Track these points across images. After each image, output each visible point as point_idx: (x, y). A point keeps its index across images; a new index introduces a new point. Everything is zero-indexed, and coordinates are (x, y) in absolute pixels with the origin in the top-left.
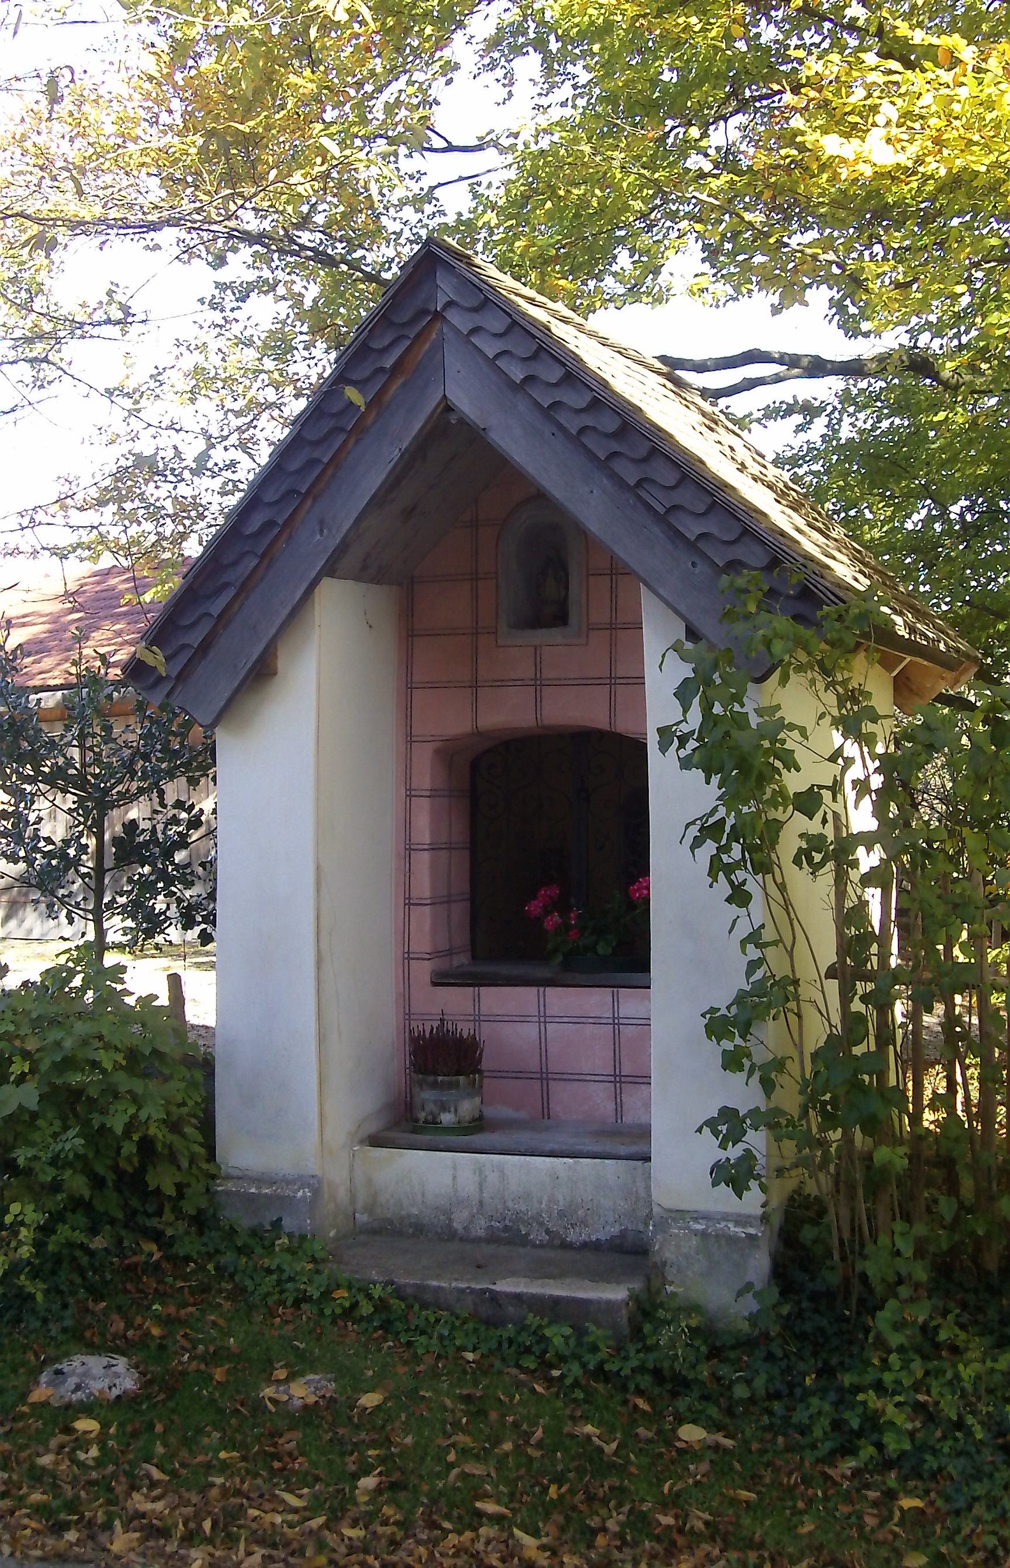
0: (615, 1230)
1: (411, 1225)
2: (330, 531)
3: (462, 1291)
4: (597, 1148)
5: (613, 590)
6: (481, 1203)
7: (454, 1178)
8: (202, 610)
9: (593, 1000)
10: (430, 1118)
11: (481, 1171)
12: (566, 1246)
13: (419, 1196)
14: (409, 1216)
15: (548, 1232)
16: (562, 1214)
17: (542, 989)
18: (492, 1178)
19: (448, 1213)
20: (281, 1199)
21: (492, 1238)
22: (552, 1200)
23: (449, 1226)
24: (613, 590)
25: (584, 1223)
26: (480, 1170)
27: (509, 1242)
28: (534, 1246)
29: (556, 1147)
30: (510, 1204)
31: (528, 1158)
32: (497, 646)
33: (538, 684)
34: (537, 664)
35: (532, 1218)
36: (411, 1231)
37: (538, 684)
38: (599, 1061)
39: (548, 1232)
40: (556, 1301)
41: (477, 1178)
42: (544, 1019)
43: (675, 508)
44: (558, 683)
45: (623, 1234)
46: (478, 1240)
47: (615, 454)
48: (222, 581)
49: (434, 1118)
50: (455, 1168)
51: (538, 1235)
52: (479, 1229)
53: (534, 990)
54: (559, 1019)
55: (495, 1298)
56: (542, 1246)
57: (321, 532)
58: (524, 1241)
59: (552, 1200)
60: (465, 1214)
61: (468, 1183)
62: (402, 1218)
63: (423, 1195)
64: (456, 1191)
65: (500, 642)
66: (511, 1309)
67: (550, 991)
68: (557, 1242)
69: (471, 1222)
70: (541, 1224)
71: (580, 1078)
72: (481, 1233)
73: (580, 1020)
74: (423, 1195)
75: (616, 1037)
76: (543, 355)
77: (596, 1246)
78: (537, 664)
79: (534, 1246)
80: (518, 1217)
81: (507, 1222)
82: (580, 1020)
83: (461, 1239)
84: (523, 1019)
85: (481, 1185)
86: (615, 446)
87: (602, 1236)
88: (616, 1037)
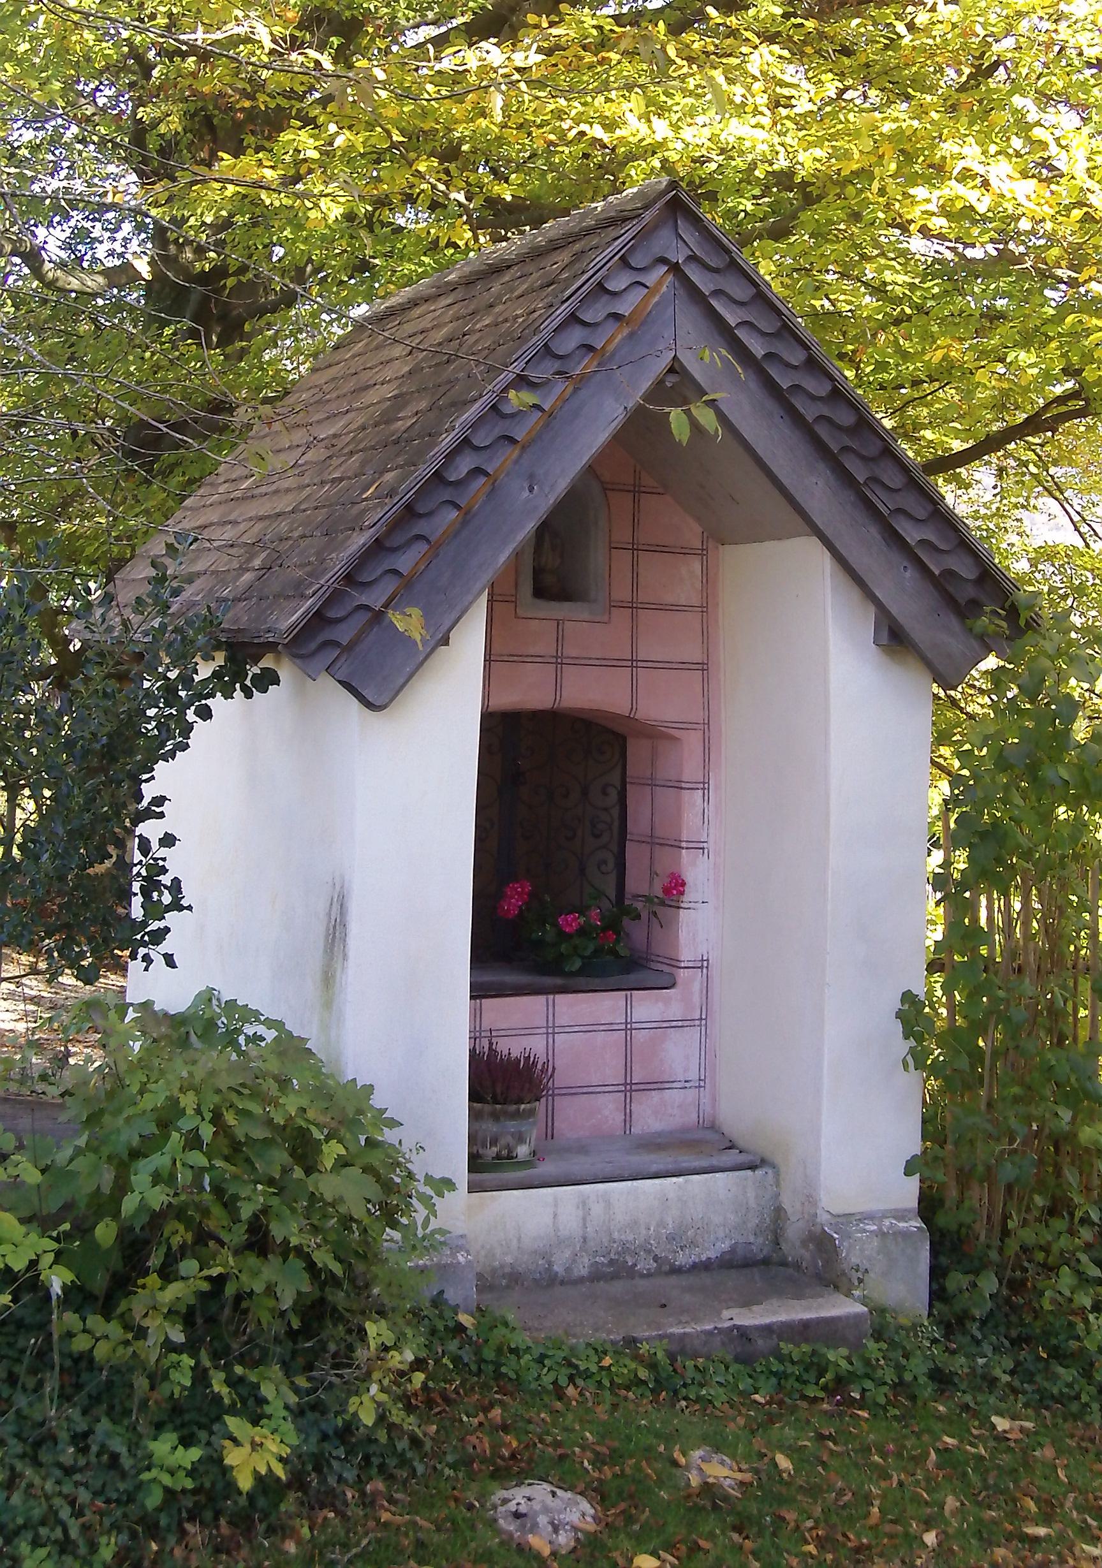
0: (725, 1246)
1: (504, 1276)
2: (541, 489)
3: (709, 1333)
4: (704, 1163)
5: (634, 566)
6: (585, 1240)
7: (555, 1215)
8: (386, 566)
9: (605, 1006)
10: (504, 1152)
11: (584, 1203)
12: (676, 1271)
13: (515, 1242)
14: (502, 1266)
15: (656, 1259)
16: (671, 1238)
17: (551, 997)
18: (597, 1210)
19: (546, 1255)
20: (443, 1268)
21: (596, 1276)
22: (661, 1224)
23: (549, 1269)
24: (634, 566)
25: (693, 1244)
26: (584, 1203)
27: (615, 1277)
28: (642, 1276)
29: (662, 1167)
30: (616, 1235)
31: (635, 1183)
32: (516, 617)
33: (559, 662)
34: (559, 640)
35: (640, 1246)
36: (504, 1282)
37: (559, 662)
38: (613, 1073)
39: (656, 1259)
40: (806, 1325)
41: (580, 1213)
42: (551, 1031)
43: (899, 511)
44: (577, 662)
45: (733, 1250)
46: (581, 1280)
47: (845, 449)
48: (416, 531)
49: (510, 1151)
50: (556, 1206)
51: (645, 1264)
52: (582, 1268)
53: (542, 999)
54: (568, 1029)
55: (743, 1334)
56: (649, 1275)
57: (531, 490)
58: (631, 1273)
59: (661, 1224)
60: (567, 1254)
61: (570, 1221)
62: (494, 1271)
63: (519, 1240)
64: (556, 1230)
65: (520, 612)
66: (760, 1342)
67: (560, 998)
68: (667, 1268)
69: (574, 1261)
70: (649, 1251)
71: (588, 1090)
72: (584, 1272)
73: (591, 1028)
74: (519, 1240)
75: (628, 1044)
76: (786, 334)
77: (705, 1266)
78: (559, 640)
79: (642, 1276)
80: (625, 1249)
81: (612, 1256)
82: (591, 1028)
83: (562, 1283)
84: (571, 1029)
85: (584, 1219)
86: (847, 441)
87: (712, 1254)
88: (628, 1044)
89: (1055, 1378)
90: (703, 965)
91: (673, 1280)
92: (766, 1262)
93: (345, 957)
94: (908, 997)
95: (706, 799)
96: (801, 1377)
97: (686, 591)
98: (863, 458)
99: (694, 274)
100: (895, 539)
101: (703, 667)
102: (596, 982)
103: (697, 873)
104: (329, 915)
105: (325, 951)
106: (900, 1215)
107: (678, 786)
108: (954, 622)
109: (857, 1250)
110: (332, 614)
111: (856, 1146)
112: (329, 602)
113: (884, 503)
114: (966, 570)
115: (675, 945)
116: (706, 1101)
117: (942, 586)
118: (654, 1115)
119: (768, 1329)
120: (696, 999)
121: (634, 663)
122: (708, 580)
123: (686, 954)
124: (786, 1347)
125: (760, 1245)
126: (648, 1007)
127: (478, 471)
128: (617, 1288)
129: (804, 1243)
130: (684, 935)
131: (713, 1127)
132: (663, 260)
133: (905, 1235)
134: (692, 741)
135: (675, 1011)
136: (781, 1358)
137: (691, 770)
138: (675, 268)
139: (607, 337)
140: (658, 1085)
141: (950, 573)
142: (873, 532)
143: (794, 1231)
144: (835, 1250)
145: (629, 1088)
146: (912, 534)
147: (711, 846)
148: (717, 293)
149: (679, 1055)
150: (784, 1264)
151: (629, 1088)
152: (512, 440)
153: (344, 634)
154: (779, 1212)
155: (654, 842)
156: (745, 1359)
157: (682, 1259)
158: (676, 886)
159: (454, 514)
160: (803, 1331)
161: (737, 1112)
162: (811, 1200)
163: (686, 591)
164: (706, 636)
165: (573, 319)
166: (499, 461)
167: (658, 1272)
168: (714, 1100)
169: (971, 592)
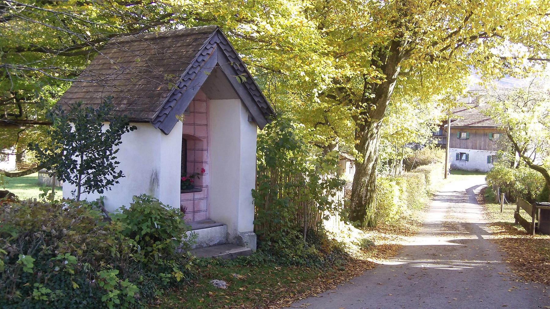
0: (218, 241)
12: (210, 246)
16: (209, 240)
22: (208, 237)
27: (200, 248)
40: (241, 252)
43: (255, 95)
45: (219, 242)
51: (205, 245)
58: (202, 247)
59: (208, 237)
77: (215, 245)
89: (282, 260)
90: (207, 186)
91: (210, 248)
92: (225, 244)
93: (158, 185)
94: (252, 190)
95: (207, 152)
96: (243, 261)
97: (203, 109)
98: (249, 84)
99: (221, 46)
100: (253, 100)
101: (207, 125)
102: (188, 191)
103: (206, 167)
104: (151, 177)
105: (150, 185)
106: (251, 232)
107: (202, 150)
108: (262, 116)
109: (245, 239)
110: (160, 115)
111: (244, 220)
112: (160, 113)
113: (252, 93)
114: (265, 107)
115: (202, 183)
116: (207, 214)
117: (260, 109)
118: (199, 217)
119: (235, 253)
120: (206, 193)
121: (194, 124)
122: (208, 108)
123: (204, 185)
124: (239, 257)
125: (224, 240)
126: (197, 195)
127: (185, 86)
128: (201, 250)
129: (234, 239)
130: (204, 181)
131: (209, 219)
132: (216, 43)
133: (253, 235)
134: (205, 141)
135: (202, 196)
136: (238, 259)
137: (205, 147)
138: (218, 44)
139: (207, 58)
140: (199, 211)
141: (262, 107)
142: (250, 99)
143: (231, 237)
144: (242, 239)
145: (194, 212)
146: (257, 99)
147: (208, 162)
148: (225, 50)
149: (203, 205)
150: (229, 243)
151: (194, 212)
152: (190, 79)
153: (161, 119)
154: (228, 234)
155: (195, 162)
156: (232, 259)
157: (211, 244)
158: (203, 171)
159: (181, 94)
160: (241, 254)
161: (214, 215)
162: (236, 230)
163: (203, 109)
164: (207, 119)
165: (201, 54)
166: (188, 84)
167: (207, 247)
168: (209, 214)
169: (266, 111)
